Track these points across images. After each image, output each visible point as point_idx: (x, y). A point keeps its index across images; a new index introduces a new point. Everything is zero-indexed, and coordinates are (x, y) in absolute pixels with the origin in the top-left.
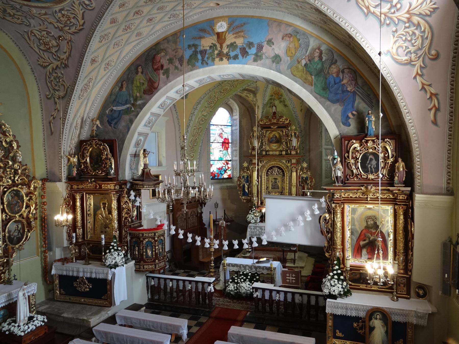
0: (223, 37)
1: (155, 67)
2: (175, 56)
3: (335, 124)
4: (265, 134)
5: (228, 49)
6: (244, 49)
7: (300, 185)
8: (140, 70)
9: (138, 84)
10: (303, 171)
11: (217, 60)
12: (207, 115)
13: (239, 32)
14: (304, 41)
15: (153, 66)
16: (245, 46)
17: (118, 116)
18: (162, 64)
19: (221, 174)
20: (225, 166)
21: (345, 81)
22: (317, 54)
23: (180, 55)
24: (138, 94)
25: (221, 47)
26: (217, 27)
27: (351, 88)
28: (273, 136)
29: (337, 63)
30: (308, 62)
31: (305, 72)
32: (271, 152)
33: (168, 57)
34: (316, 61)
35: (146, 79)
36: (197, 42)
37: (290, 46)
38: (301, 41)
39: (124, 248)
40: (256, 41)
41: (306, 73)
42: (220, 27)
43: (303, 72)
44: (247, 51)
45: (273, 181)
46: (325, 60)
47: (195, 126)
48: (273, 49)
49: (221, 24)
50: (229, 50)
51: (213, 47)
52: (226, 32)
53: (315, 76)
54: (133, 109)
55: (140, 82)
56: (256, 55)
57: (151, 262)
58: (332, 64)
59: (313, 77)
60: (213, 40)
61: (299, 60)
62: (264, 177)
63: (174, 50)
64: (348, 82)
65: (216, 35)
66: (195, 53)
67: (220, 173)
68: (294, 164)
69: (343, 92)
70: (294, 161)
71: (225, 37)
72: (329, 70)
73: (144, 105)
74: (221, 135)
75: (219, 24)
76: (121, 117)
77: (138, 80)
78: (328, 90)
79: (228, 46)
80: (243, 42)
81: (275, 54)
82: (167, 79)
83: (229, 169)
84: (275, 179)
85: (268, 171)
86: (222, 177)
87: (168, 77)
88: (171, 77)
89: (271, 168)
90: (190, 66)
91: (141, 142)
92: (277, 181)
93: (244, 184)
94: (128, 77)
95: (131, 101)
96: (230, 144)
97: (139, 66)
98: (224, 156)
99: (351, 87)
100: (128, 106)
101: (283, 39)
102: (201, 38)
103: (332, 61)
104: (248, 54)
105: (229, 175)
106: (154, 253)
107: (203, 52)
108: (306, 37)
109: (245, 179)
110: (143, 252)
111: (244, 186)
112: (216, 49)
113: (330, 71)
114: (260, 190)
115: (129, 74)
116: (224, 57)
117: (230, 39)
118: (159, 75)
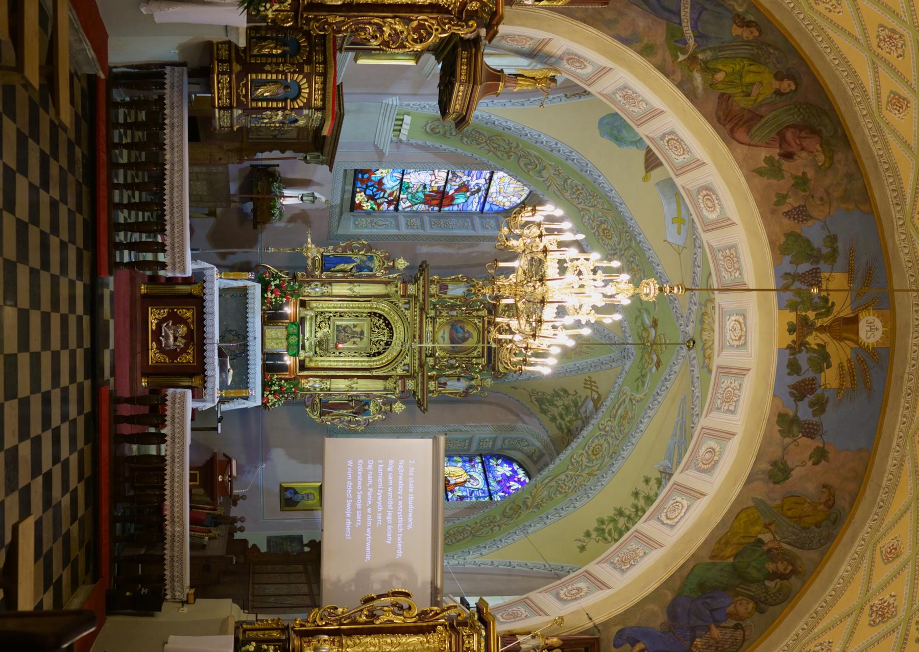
0: (845, 335)
1: (789, 135)
2: (813, 197)
3: (621, 614)
4: (474, 313)
5: (816, 347)
6: (812, 389)
7: (350, 396)
8: (787, 86)
9: (748, 79)
10: (384, 404)
11: (792, 317)
12: (542, 177)
13: (854, 376)
14: (814, 537)
15: (794, 126)
16: (819, 391)
17: (664, 8)
18: (796, 157)
19: (367, 187)
20: (386, 196)
21: (715, 632)
22: (781, 567)
23: (815, 214)
24: (720, 76)
25: (822, 329)
26: (871, 318)
27: (699, 646)
28: (468, 332)
29: (757, 613)
30: (765, 548)
31: (743, 541)
32: (431, 329)
33: (810, 174)
34: (766, 566)
35: (761, 105)
36: (841, 261)
37: (806, 505)
38: (816, 530)
39: (288, 17)
40: (828, 419)
41: (741, 544)
42: (870, 324)
43: (743, 537)
44: (805, 396)
45: (358, 330)
46: (766, 588)
47: (518, 145)
48: (803, 464)
49: (877, 329)
50: (814, 351)
51: (823, 308)
52: (856, 342)
53: (733, 565)
54: (681, 58)
55: (752, 84)
56: (795, 420)
57: (238, 96)
58: (756, 603)
59: (731, 560)
60: (842, 306)
61: (772, 528)
62: (365, 308)
63: (828, 194)
64: (713, 639)
65: (852, 315)
66: (814, 256)
67: (369, 184)
68: (404, 385)
69: (693, 629)
70: (410, 384)
71: (846, 339)
72: (743, 596)
73: (691, 94)
74: (464, 188)
75: (878, 324)
76: (662, 18)
77: (758, 78)
78: (700, 594)
79: (822, 347)
80: (828, 387)
81: (792, 470)
82: (753, 171)
83: (375, 207)
84: (362, 333)
85: (380, 316)
86: (358, 190)
87: (759, 172)
88: (757, 180)
89: (388, 325)
90: (783, 239)
91: (576, 67)
92: (355, 339)
93: (354, 262)
94: (769, 45)
95: (704, 51)
96: (436, 209)
97: (796, 84)
98: (410, 195)
99: (702, 645)
100: (691, 42)
101: (824, 486)
102: (850, 271)
103: (763, 603)
104: (799, 400)
105: (360, 206)
106: (265, 104)
107: (813, 278)
108: (822, 541)
109: (364, 262)
110: (267, 72)
111: (348, 260)
112: (818, 316)
113: (740, 598)
114: (338, 299)
115: (776, 49)
116: (798, 337)
117: (839, 352)
118: (768, 145)
